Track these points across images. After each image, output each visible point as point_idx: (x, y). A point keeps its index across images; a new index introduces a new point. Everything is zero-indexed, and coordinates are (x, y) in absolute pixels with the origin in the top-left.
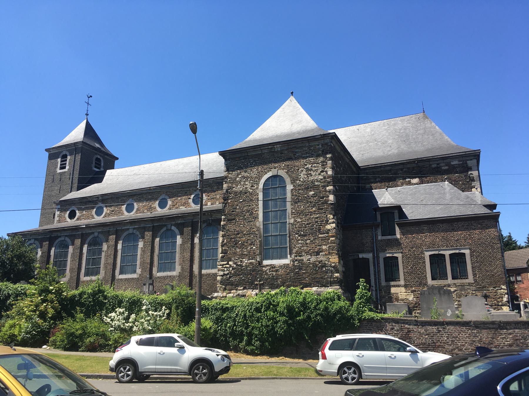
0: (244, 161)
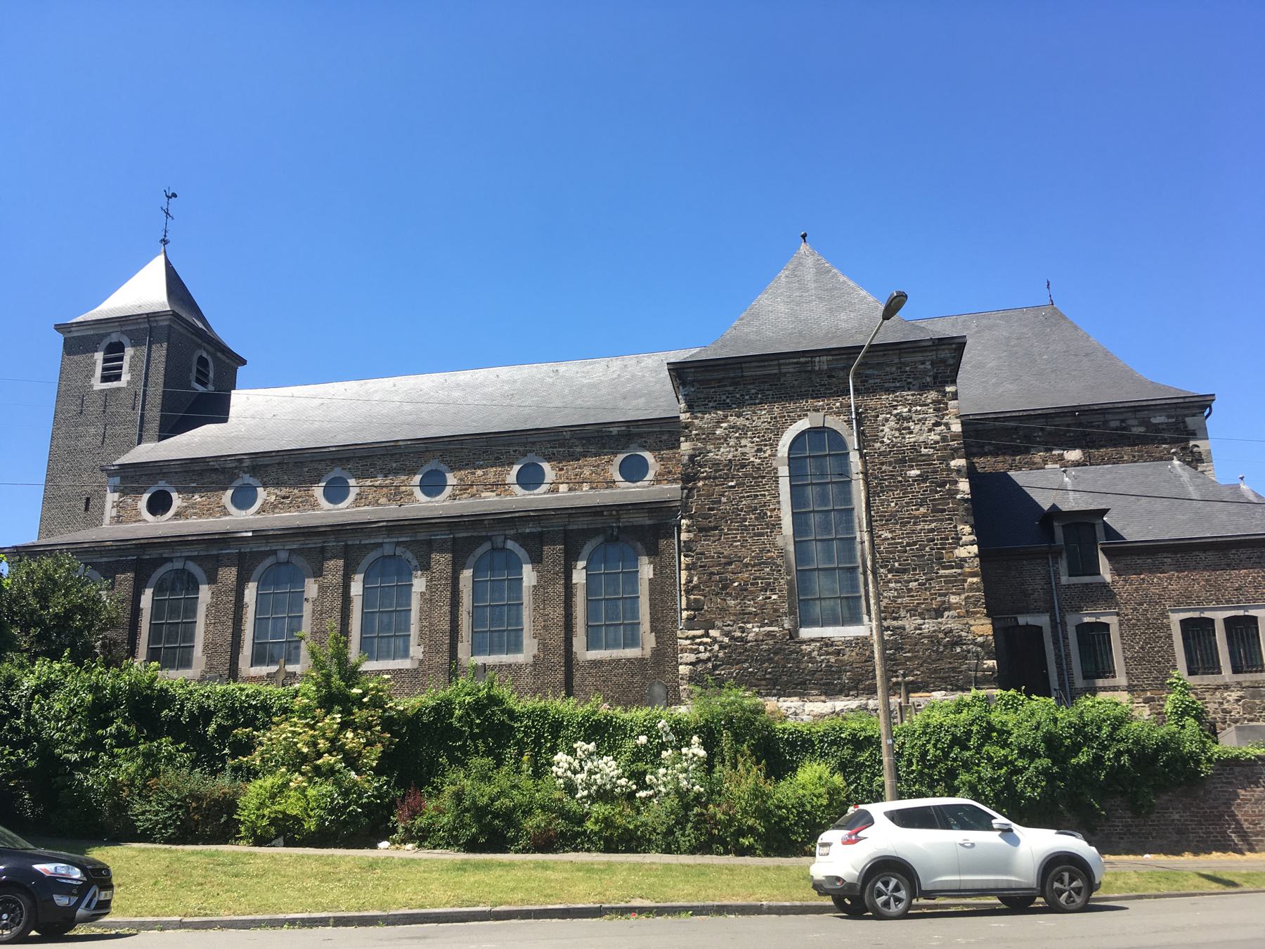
0: (731, 388)
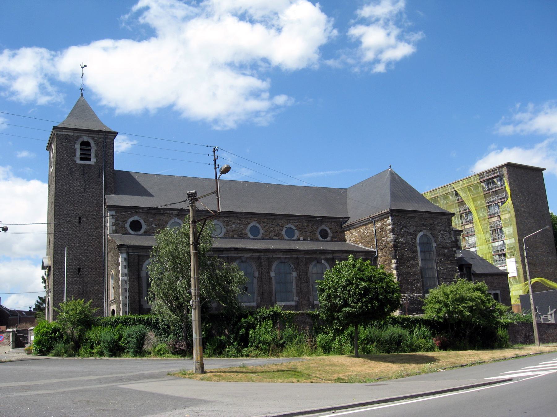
0: (403, 219)
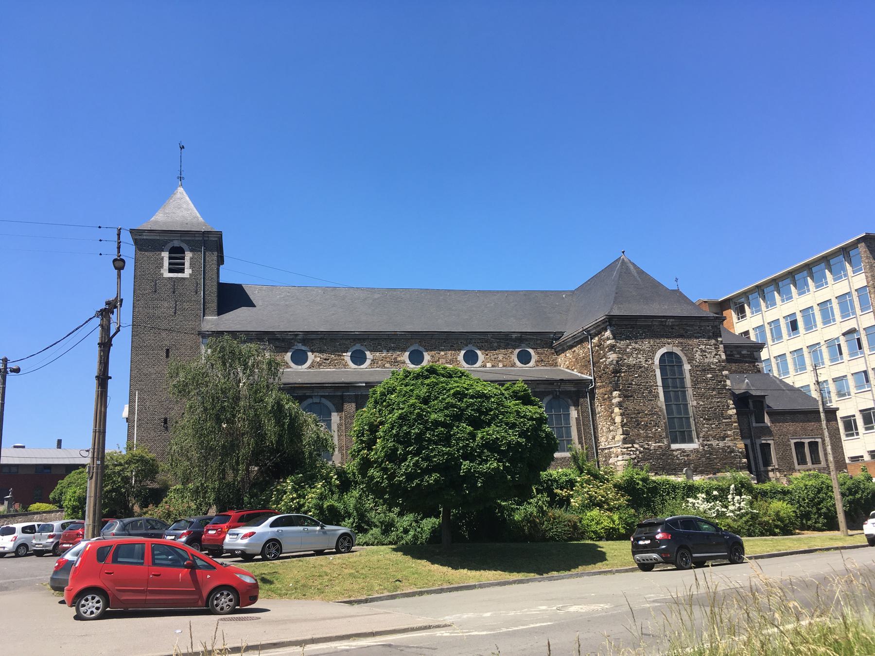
0: (631, 330)
